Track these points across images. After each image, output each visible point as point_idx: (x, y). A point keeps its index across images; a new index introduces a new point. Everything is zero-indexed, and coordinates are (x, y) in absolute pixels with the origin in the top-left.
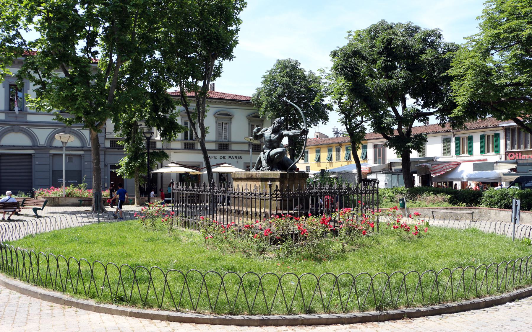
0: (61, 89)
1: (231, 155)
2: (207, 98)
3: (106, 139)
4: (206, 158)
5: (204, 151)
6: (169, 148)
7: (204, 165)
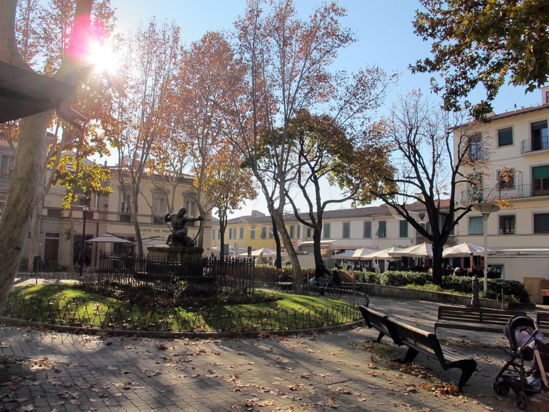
2: (278, 262)
3: (44, 207)
6: (106, 219)
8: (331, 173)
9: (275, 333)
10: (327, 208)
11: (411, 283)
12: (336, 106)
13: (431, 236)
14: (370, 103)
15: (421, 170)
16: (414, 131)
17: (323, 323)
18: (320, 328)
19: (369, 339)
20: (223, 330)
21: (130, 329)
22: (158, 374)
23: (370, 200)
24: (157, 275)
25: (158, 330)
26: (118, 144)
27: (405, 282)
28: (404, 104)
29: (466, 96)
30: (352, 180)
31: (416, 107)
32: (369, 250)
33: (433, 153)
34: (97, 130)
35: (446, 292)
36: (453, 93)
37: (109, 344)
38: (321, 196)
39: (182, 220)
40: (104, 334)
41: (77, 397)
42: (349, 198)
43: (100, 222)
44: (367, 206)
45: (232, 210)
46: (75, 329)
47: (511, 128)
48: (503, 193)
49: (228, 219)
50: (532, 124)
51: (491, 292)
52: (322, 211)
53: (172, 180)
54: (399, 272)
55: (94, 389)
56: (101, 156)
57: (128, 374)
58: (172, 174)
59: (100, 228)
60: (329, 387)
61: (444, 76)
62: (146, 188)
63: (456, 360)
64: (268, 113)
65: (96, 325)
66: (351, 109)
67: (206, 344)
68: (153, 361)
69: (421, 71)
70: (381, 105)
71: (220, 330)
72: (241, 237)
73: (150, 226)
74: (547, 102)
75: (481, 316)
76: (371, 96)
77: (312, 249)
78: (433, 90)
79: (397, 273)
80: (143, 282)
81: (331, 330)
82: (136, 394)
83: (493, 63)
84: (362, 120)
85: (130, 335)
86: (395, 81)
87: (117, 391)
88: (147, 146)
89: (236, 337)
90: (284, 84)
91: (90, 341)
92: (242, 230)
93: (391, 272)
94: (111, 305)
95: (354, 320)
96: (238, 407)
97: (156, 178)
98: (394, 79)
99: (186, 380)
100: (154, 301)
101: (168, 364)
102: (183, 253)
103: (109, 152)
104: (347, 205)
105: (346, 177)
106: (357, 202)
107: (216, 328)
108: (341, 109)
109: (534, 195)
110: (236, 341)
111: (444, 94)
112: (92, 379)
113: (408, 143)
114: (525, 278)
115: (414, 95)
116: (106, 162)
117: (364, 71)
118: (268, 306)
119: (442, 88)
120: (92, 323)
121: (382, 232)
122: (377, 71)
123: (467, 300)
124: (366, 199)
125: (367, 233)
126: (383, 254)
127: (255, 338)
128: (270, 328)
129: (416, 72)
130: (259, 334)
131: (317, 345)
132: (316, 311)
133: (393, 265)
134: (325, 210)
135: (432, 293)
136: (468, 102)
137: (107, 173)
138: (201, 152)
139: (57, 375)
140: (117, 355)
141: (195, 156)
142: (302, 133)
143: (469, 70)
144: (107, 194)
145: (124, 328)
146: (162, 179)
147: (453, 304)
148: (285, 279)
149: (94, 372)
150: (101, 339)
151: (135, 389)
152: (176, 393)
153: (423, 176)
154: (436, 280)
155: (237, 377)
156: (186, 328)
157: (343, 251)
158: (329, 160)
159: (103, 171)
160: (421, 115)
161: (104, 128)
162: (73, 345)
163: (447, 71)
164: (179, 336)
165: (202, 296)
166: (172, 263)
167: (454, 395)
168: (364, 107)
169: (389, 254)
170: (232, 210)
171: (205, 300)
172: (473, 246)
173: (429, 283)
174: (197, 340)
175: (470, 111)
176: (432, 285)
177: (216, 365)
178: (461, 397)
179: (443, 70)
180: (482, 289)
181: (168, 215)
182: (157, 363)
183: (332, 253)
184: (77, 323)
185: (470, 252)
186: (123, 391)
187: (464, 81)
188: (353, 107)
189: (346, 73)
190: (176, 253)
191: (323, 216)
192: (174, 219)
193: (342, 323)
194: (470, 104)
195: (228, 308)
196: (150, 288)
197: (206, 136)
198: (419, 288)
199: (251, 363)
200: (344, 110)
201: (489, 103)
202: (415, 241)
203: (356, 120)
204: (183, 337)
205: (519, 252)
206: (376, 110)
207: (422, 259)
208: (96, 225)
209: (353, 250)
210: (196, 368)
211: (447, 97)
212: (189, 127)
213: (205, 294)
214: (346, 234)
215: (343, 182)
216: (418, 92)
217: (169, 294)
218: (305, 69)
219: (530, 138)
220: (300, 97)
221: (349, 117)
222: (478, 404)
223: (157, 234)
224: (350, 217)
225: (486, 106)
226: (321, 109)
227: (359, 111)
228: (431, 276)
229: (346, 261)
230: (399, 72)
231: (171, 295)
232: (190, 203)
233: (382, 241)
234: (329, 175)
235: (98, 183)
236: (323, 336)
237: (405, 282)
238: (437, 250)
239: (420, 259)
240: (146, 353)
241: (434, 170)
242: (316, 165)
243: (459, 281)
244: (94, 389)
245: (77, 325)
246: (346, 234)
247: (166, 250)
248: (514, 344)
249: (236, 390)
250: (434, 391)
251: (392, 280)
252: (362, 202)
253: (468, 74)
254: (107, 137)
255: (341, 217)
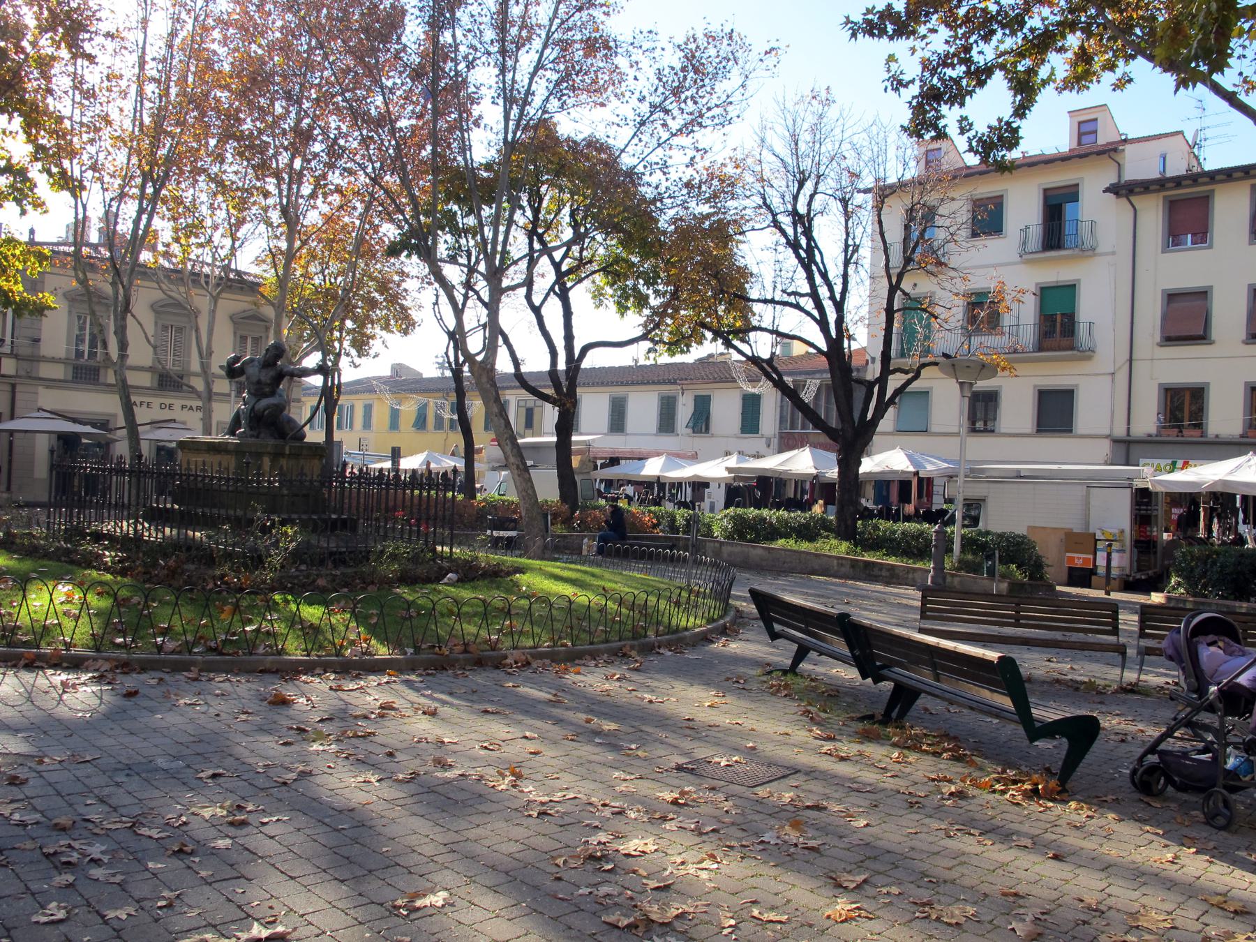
0: (606, 163)
1: (188, 403)
4: (128, 408)
5: (124, 391)
7: (121, 422)
8: (599, 278)
9: (541, 656)
10: (593, 360)
11: (787, 536)
12: (631, 116)
13: (835, 430)
14: (710, 114)
15: (818, 280)
16: (809, 186)
17: (645, 629)
18: (642, 640)
19: (769, 669)
20: (418, 650)
21: (173, 652)
22: (304, 775)
23: (688, 346)
24: (207, 511)
25: (251, 654)
26: (66, 182)
27: (774, 532)
28: (790, 123)
29: (962, 105)
30: (647, 297)
31: (814, 129)
32: (677, 460)
33: (846, 240)
34: (9, 143)
35: (868, 557)
36: (932, 95)
37: (131, 695)
38: (575, 332)
39: (272, 373)
40: (107, 666)
41: (106, 859)
42: (644, 337)
43: (18, 380)
44: (679, 358)
45: (357, 361)
46: (20, 657)
47: (1002, 196)
48: (976, 341)
49: (343, 380)
50: (1045, 190)
51: (970, 557)
52: (578, 368)
53: (207, 283)
54: (757, 511)
55: (144, 831)
56: (24, 212)
57: (221, 780)
58: (206, 270)
59: (18, 396)
60: (762, 792)
61: (919, 54)
62: (144, 297)
63: (1057, 717)
64: (460, 126)
65: (79, 643)
66: (665, 125)
67: (386, 687)
68: (271, 738)
69: (872, 35)
70: (735, 119)
71: (410, 651)
72: (367, 424)
73: (150, 395)
74: (1079, 144)
75: (1018, 612)
76: (714, 96)
77: (553, 456)
78: (889, 84)
79: (752, 512)
80: (167, 530)
81: (668, 645)
82: (272, 837)
83: (1032, 30)
84: (691, 153)
85: (178, 667)
86: (771, 66)
87: (212, 832)
88: (149, 190)
89: (452, 666)
90: (506, 52)
91: (74, 686)
92: (368, 409)
93: (740, 511)
94: (105, 590)
95: (711, 620)
96: (573, 863)
97: (168, 277)
98: (770, 60)
99: (389, 792)
100: (214, 578)
101: (316, 747)
102: (276, 455)
103: (44, 203)
104: (638, 354)
105: (635, 288)
106: (660, 347)
107: (397, 644)
108: (642, 123)
109: (1040, 348)
110: (456, 676)
111: (914, 97)
112: (128, 800)
113: (794, 213)
114: (1029, 527)
115: (814, 102)
116: (32, 232)
117: (700, 36)
118: (498, 588)
119: (913, 81)
120: (68, 639)
121: (701, 420)
122: (731, 38)
123: (918, 576)
124: (679, 342)
125: (667, 423)
126: (715, 469)
127: (497, 667)
128: (530, 643)
129: (860, 36)
130: (506, 657)
131: (656, 684)
132: (621, 602)
133: (735, 494)
134: (586, 364)
135: (839, 558)
136: (966, 119)
137: (41, 257)
138: (284, 212)
139: (15, 792)
140: (164, 724)
141: (269, 224)
142: (538, 183)
143: (976, 42)
144: (40, 310)
145: (160, 648)
146: (182, 279)
147: (887, 583)
148: (500, 525)
149: (124, 779)
150: (99, 679)
151: (264, 824)
152: (379, 829)
153: (823, 292)
154: (846, 531)
155: (519, 776)
156: (321, 647)
157: (614, 461)
158: (601, 246)
159: (29, 252)
160: (828, 148)
161: (29, 141)
162: (30, 699)
163: (927, 40)
164: (309, 668)
165: (330, 565)
166: (259, 482)
167: (1053, 800)
168: (695, 122)
169: (727, 469)
170: (357, 361)
171: (338, 573)
172: (917, 456)
173: (827, 537)
174: (358, 677)
175: (970, 141)
176: (834, 542)
177: (443, 742)
178: (1073, 804)
179: (915, 39)
180: (949, 550)
181: (237, 359)
182: (285, 744)
183: (592, 465)
184: (24, 639)
185: (911, 469)
186: (232, 831)
187: (963, 68)
188: (670, 122)
189: (658, 37)
190: (258, 455)
191: (580, 379)
192: (253, 371)
193: (686, 629)
194: (971, 125)
195: (404, 592)
196: (189, 546)
197: (297, 177)
198: (805, 546)
199: (528, 734)
200: (648, 128)
201: (1014, 125)
202: (775, 442)
203: (674, 153)
204: (318, 671)
205: (1018, 471)
206: (723, 131)
207: (803, 482)
208: (8, 388)
209: (640, 459)
210: (397, 754)
211: (920, 105)
212: (252, 149)
213: (338, 559)
214: (617, 422)
215: (627, 299)
216: (824, 95)
217: (252, 558)
218: (557, 21)
219: (1040, 222)
220: (540, 89)
221: (659, 145)
222: (1120, 820)
223: (166, 415)
224: (627, 384)
225: (1006, 131)
226: (588, 122)
227: (685, 130)
228: (831, 521)
229: (621, 483)
230: (782, 45)
231: (257, 560)
232: (249, 341)
233: (699, 442)
234: (594, 282)
235: (16, 283)
236: (654, 660)
237: (774, 532)
238: (849, 462)
239: (800, 481)
240: (244, 717)
241: (845, 276)
242: (565, 256)
243: (894, 532)
244: (144, 831)
245: (25, 644)
246: (617, 422)
247: (231, 448)
248: (1197, 678)
249: (539, 814)
250: (1003, 792)
251: (742, 529)
252: (669, 349)
253: (974, 53)
254: (39, 165)
255: (607, 385)
